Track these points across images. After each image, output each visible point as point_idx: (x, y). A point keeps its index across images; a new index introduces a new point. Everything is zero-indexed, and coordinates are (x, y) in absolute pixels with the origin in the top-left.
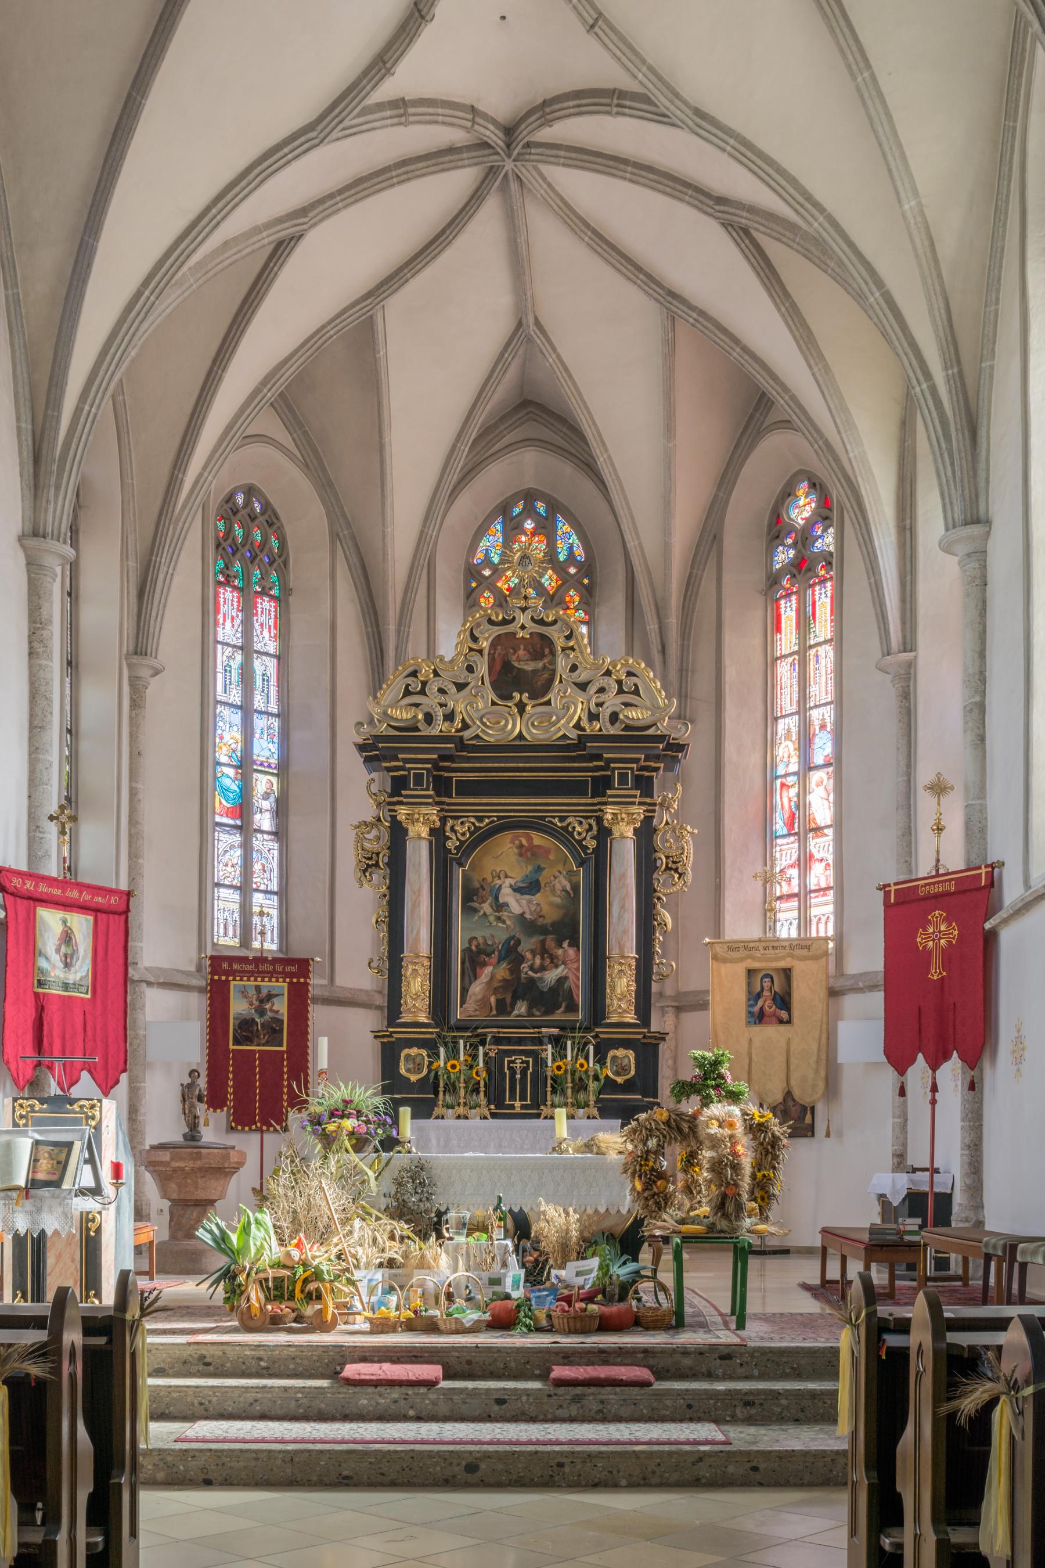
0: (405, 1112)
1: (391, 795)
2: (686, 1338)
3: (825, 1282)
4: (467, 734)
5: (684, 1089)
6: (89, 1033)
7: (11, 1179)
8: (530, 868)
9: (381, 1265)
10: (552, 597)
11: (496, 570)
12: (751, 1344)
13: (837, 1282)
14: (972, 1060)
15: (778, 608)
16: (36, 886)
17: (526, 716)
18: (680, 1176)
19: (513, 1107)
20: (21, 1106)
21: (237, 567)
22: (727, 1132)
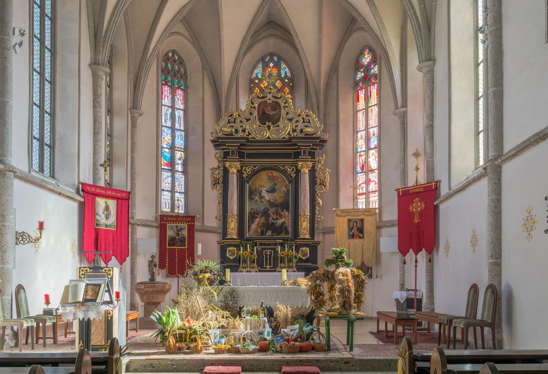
0: (228, 271)
1: (223, 158)
2: (332, 355)
3: (379, 331)
4: (250, 137)
5: (329, 262)
6: (115, 243)
7: (76, 299)
8: (272, 184)
9: (219, 328)
10: (280, 90)
11: (261, 81)
12: (356, 358)
13: (384, 331)
14: (430, 251)
15: (358, 93)
16: (96, 190)
17: (271, 130)
18: (328, 294)
19: (266, 268)
20: (82, 270)
21: (169, 79)
22: (345, 278)
